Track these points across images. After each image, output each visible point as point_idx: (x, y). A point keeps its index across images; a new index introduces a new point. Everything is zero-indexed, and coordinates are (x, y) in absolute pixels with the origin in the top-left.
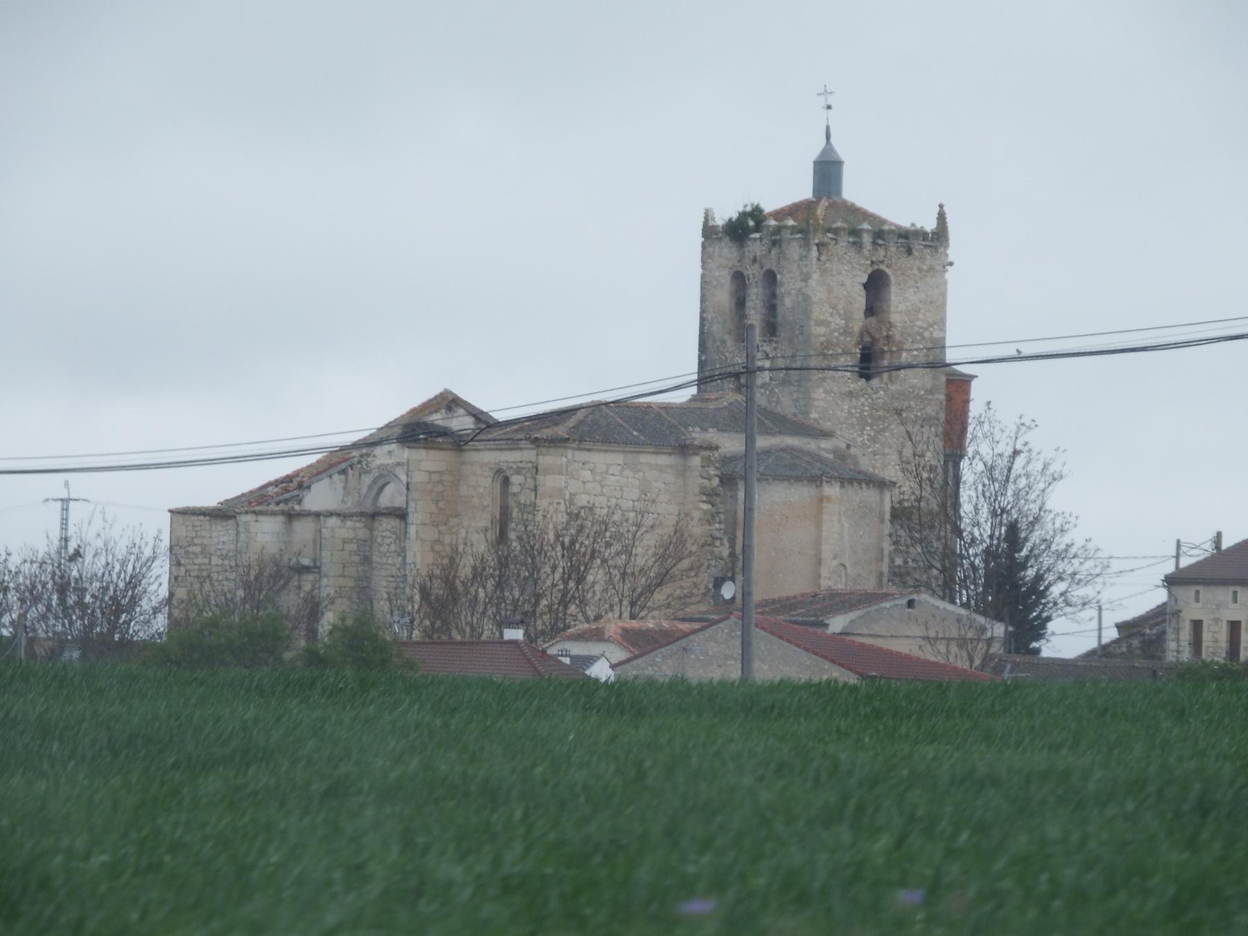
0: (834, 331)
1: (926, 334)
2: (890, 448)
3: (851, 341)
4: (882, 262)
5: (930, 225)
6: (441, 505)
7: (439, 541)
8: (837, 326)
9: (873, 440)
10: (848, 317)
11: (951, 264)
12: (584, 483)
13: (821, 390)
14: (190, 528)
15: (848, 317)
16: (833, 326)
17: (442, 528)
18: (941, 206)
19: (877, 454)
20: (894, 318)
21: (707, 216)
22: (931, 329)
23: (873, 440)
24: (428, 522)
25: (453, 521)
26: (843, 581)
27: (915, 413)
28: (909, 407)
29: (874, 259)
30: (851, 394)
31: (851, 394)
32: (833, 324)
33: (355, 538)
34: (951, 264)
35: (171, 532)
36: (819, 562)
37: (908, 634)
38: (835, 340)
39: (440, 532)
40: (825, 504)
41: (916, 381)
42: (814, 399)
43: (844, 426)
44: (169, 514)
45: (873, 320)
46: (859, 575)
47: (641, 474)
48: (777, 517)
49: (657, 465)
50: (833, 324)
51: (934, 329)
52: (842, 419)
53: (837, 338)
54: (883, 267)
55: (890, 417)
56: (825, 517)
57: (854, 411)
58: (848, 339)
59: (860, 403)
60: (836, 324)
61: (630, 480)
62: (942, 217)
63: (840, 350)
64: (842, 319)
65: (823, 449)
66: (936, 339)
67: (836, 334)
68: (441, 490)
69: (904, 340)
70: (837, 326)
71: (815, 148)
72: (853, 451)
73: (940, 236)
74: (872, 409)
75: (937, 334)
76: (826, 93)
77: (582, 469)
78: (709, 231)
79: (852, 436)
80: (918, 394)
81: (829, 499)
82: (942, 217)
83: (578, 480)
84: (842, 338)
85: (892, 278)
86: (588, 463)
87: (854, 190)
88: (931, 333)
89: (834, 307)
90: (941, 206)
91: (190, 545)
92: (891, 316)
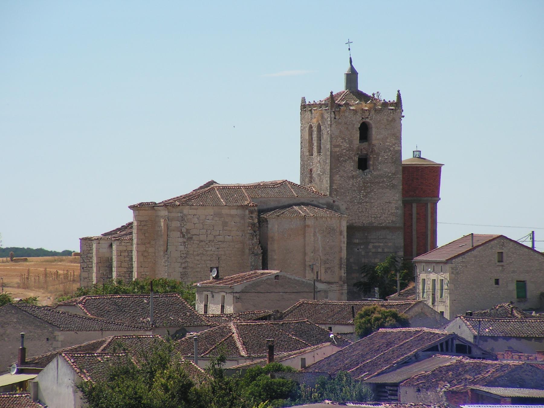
0: (344, 149)
1: (392, 149)
2: (374, 199)
3: (352, 154)
4: (367, 118)
5: (394, 99)
6: (147, 235)
7: (145, 251)
8: (345, 148)
9: (365, 196)
10: (351, 142)
11: (403, 117)
12: (195, 224)
13: (338, 176)
14: (88, 246)
15: (351, 142)
16: (343, 147)
17: (148, 245)
18: (399, 91)
19: (368, 203)
20: (374, 142)
21: (304, 100)
22: (394, 146)
23: (365, 196)
24: (140, 243)
25: (153, 242)
26: (319, 263)
27: (386, 184)
28: (384, 181)
29: (363, 117)
30: (353, 177)
31: (353, 177)
32: (343, 146)
33: (126, 250)
34: (403, 117)
35: (81, 248)
36: (305, 254)
37: (276, 291)
38: (344, 154)
39: (146, 247)
40: (307, 229)
41: (386, 169)
42: (334, 180)
43: (350, 191)
44: (80, 240)
45: (365, 145)
46: (327, 259)
47: (223, 219)
48: (286, 235)
49: (230, 214)
50: (343, 146)
51: (396, 146)
52: (349, 188)
53: (345, 152)
54: (368, 120)
55: (374, 186)
56: (307, 234)
57: (355, 184)
58: (351, 153)
59: (358, 181)
60: (344, 147)
61: (217, 222)
62: (399, 96)
63: (347, 158)
64: (347, 144)
65: (321, 203)
66: (396, 150)
67: (345, 151)
68: (146, 228)
69: (380, 152)
70: (345, 148)
71: (346, 69)
72: (336, 203)
73: (398, 104)
74: (364, 183)
75: (397, 148)
76: (349, 43)
77: (193, 218)
78: (305, 107)
79: (354, 195)
80: (388, 175)
81: (308, 226)
82: (399, 96)
83: (191, 223)
84: (348, 152)
85: (373, 125)
86: (196, 215)
87: (362, 87)
88: (394, 148)
89: (343, 139)
90: (399, 91)
91: (88, 254)
92: (373, 141)
